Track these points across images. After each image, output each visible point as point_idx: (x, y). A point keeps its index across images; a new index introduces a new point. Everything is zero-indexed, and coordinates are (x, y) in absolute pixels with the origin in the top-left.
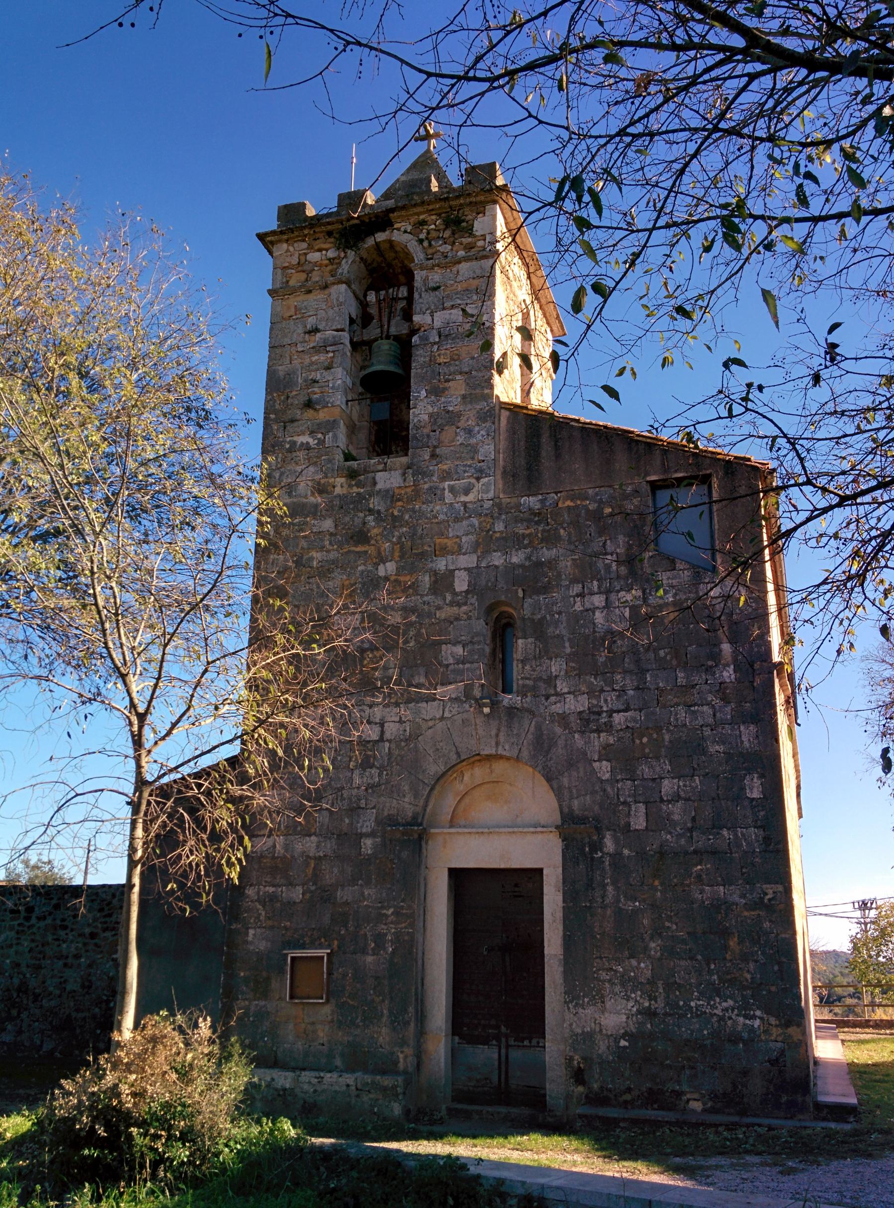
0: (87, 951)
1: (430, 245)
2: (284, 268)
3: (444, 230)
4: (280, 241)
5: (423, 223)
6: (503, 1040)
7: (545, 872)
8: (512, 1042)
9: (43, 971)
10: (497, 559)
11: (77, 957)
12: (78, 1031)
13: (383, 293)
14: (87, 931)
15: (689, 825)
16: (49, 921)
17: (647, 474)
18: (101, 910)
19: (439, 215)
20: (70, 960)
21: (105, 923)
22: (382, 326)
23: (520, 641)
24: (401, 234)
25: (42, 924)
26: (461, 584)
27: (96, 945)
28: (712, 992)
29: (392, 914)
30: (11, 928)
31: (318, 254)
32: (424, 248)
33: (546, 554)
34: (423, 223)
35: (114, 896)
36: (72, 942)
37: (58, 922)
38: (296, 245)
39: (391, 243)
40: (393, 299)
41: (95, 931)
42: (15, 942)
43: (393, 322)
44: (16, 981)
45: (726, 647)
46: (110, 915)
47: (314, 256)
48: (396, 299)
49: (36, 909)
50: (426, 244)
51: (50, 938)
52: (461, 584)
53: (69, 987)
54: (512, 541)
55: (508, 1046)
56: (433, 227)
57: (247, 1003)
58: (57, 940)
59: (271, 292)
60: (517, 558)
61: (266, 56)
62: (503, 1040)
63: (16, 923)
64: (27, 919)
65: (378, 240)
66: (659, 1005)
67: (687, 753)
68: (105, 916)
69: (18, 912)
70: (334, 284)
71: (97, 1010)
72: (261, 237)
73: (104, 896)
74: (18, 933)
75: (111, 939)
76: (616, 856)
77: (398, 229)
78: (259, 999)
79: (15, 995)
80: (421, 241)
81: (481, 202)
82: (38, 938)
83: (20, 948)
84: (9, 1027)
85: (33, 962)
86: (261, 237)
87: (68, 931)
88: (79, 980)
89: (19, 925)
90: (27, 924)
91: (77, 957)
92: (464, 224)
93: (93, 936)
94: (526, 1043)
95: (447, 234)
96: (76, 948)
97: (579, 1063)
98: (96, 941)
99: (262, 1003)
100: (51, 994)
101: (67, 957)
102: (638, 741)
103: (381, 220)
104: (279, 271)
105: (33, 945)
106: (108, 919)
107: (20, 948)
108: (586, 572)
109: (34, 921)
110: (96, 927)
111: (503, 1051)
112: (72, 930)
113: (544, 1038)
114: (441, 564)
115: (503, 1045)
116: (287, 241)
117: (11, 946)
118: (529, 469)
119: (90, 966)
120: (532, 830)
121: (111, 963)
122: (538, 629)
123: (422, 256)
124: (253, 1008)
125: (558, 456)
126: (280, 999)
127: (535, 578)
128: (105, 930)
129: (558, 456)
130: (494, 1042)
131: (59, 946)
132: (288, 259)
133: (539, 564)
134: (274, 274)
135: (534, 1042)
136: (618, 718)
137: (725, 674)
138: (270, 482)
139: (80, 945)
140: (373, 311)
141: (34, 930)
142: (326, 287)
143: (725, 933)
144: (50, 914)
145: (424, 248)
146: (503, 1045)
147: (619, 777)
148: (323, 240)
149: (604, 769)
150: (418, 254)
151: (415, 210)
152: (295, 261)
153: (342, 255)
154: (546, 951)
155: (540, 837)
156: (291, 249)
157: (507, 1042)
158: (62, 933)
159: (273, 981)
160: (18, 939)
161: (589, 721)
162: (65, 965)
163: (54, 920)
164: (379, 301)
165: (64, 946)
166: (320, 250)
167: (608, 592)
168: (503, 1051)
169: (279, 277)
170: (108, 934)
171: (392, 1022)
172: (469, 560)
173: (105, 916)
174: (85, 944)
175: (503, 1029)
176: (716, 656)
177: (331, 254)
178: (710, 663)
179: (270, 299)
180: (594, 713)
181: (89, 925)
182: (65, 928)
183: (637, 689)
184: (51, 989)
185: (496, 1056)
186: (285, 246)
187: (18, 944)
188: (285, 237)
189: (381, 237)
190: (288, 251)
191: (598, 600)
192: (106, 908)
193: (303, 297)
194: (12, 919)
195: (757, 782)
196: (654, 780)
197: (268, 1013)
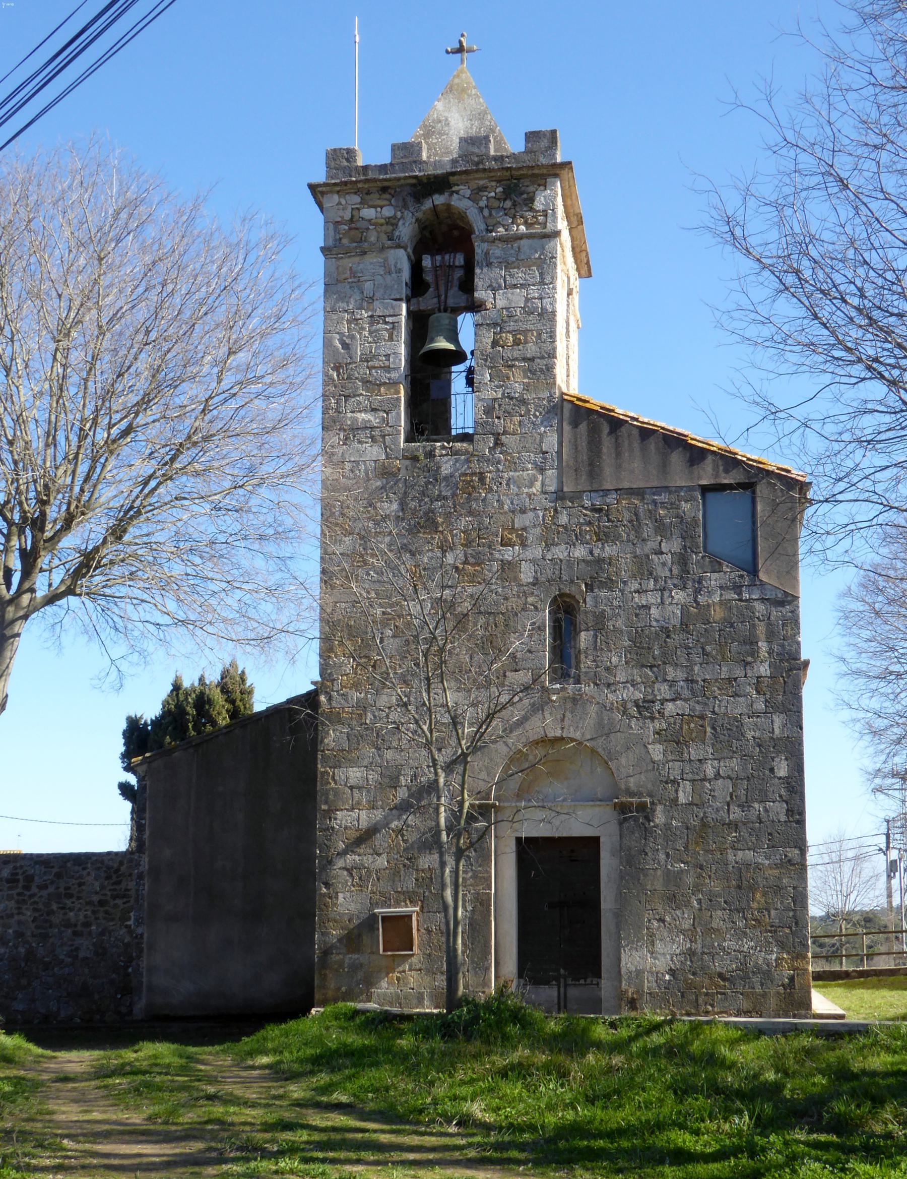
0: (97, 919)
1: (491, 214)
2: (337, 223)
3: (505, 200)
4: (331, 192)
5: (484, 188)
6: (562, 980)
7: (601, 840)
8: (570, 982)
9: (51, 940)
10: (560, 552)
11: (87, 925)
12: (96, 997)
13: (438, 258)
14: (95, 898)
15: (728, 799)
16: (51, 889)
17: (700, 478)
18: (108, 878)
19: (499, 181)
20: (79, 928)
21: (115, 890)
22: (439, 296)
23: (583, 634)
24: (461, 201)
25: (44, 893)
26: (526, 574)
27: (106, 912)
28: (741, 935)
29: (471, 877)
30: (10, 898)
31: (372, 210)
32: (484, 217)
33: (609, 550)
34: (484, 188)
35: (121, 863)
36: (80, 910)
37: (62, 890)
38: (348, 197)
39: (448, 207)
40: (450, 266)
41: (103, 898)
42: (15, 912)
43: (451, 293)
44: (22, 950)
45: (763, 646)
46: (119, 883)
47: (368, 213)
48: (452, 267)
49: (36, 878)
50: (486, 212)
51: (54, 907)
52: (526, 574)
53: (81, 954)
54: (574, 537)
55: (566, 986)
56: (493, 194)
57: (341, 956)
58: (63, 908)
59: (323, 249)
60: (580, 552)
61: (566, 307)
62: (562, 980)
63: (14, 892)
64: (27, 888)
65: (436, 203)
66: (698, 947)
67: (727, 735)
68: (114, 884)
69: (18, 881)
70: (392, 247)
71: (114, 976)
72: (313, 188)
73: (110, 863)
74: (18, 902)
75: (122, 906)
76: (667, 826)
77: (457, 192)
78: (353, 952)
79: (23, 965)
80: (481, 209)
81: (542, 175)
82: (41, 906)
83: (22, 918)
84: (20, 996)
85: (40, 931)
86: (313, 188)
87: (74, 899)
88: (91, 948)
89: (19, 894)
90: (28, 893)
91: (87, 925)
92: (525, 196)
93: (102, 903)
94: (582, 981)
95: (508, 204)
96: (86, 916)
97: (633, 993)
98: (107, 908)
99: (355, 956)
100: (63, 961)
101: (76, 925)
102: (685, 727)
103: (440, 183)
104: (331, 226)
105: (37, 915)
106: (117, 887)
107: (22, 918)
108: (643, 568)
109: (34, 890)
110: (105, 895)
111: (562, 990)
112: (79, 898)
113: (600, 977)
114: (508, 554)
115: (562, 984)
116: (338, 192)
117: (11, 916)
118: (591, 464)
119: (102, 933)
120: (591, 803)
121: (124, 930)
122: (599, 623)
123: (483, 227)
124: (347, 961)
125: (618, 455)
126: (372, 953)
127: (598, 575)
128: (114, 897)
129: (618, 455)
130: (554, 982)
131: (65, 914)
132: (341, 213)
133: (600, 561)
134: (326, 229)
135: (589, 981)
136: (670, 706)
137: (762, 669)
138: (328, 454)
139: (89, 913)
140: (429, 278)
141: (36, 899)
142: (383, 249)
143: (753, 889)
144: (52, 883)
145: (484, 217)
146: (562, 984)
147: (670, 758)
148: (377, 196)
149: (657, 752)
150: (478, 225)
151: (477, 176)
152: (348, 216)
153: (399, 214)
154: (602, 907)
155: (597, 809)
156: (343, 202)
157: (565, 981)
158: (68, 902)
159: (364, 937)
160: (19, 908)
161: (644, 707)
162: (75, 934)
163: (58, 888)
164: (435, 268)
165: (72, 914)
166: (375, 207)
167: (663, 590)
168: (562, 990)
169: (332, 233)
170: (119, 902)
171: (475, 969)
172: (536, 552)
173: (114, 884)
174: (94, 912)
175: (562, 971)
176: (754, 653)
177: (388, 212)
178: (749, 659)
179: (321, 258)
180: (649, 701)
181: (97, 893)
182: (70, 896)
183: (687, 680)
184: (62, 957)
185: (556, 994)
186: (336, 197)
187: (19, 914)
188: (338, 188)
189: (439, 199)
190: (339, 203)
191: (652, 598)
192: (114, 876)
193: (356, 259)
194: (10, 889)
195: (784, 764)
196: (700, 761)
197: (361, 965)
